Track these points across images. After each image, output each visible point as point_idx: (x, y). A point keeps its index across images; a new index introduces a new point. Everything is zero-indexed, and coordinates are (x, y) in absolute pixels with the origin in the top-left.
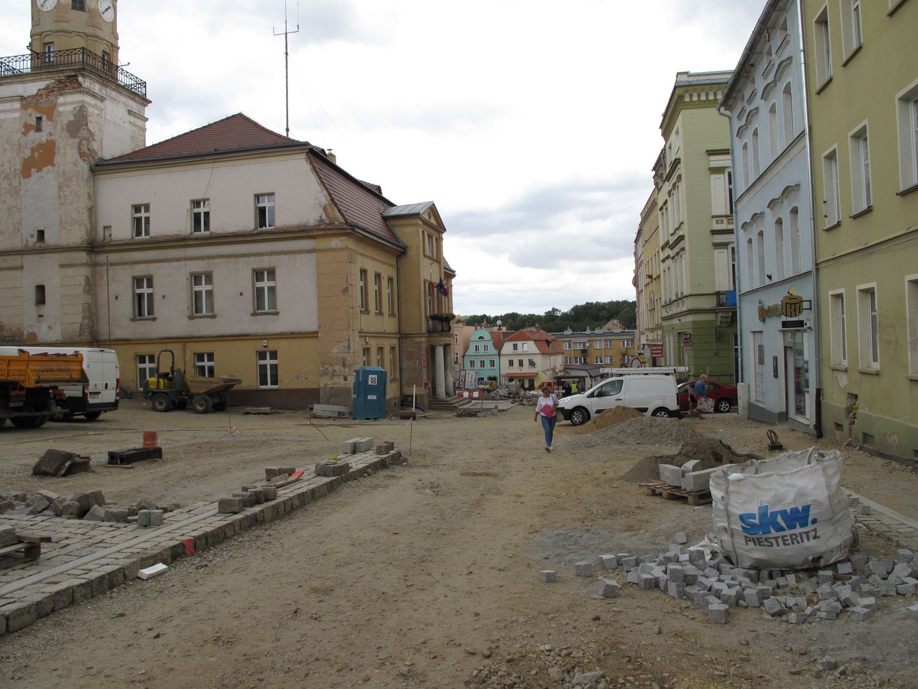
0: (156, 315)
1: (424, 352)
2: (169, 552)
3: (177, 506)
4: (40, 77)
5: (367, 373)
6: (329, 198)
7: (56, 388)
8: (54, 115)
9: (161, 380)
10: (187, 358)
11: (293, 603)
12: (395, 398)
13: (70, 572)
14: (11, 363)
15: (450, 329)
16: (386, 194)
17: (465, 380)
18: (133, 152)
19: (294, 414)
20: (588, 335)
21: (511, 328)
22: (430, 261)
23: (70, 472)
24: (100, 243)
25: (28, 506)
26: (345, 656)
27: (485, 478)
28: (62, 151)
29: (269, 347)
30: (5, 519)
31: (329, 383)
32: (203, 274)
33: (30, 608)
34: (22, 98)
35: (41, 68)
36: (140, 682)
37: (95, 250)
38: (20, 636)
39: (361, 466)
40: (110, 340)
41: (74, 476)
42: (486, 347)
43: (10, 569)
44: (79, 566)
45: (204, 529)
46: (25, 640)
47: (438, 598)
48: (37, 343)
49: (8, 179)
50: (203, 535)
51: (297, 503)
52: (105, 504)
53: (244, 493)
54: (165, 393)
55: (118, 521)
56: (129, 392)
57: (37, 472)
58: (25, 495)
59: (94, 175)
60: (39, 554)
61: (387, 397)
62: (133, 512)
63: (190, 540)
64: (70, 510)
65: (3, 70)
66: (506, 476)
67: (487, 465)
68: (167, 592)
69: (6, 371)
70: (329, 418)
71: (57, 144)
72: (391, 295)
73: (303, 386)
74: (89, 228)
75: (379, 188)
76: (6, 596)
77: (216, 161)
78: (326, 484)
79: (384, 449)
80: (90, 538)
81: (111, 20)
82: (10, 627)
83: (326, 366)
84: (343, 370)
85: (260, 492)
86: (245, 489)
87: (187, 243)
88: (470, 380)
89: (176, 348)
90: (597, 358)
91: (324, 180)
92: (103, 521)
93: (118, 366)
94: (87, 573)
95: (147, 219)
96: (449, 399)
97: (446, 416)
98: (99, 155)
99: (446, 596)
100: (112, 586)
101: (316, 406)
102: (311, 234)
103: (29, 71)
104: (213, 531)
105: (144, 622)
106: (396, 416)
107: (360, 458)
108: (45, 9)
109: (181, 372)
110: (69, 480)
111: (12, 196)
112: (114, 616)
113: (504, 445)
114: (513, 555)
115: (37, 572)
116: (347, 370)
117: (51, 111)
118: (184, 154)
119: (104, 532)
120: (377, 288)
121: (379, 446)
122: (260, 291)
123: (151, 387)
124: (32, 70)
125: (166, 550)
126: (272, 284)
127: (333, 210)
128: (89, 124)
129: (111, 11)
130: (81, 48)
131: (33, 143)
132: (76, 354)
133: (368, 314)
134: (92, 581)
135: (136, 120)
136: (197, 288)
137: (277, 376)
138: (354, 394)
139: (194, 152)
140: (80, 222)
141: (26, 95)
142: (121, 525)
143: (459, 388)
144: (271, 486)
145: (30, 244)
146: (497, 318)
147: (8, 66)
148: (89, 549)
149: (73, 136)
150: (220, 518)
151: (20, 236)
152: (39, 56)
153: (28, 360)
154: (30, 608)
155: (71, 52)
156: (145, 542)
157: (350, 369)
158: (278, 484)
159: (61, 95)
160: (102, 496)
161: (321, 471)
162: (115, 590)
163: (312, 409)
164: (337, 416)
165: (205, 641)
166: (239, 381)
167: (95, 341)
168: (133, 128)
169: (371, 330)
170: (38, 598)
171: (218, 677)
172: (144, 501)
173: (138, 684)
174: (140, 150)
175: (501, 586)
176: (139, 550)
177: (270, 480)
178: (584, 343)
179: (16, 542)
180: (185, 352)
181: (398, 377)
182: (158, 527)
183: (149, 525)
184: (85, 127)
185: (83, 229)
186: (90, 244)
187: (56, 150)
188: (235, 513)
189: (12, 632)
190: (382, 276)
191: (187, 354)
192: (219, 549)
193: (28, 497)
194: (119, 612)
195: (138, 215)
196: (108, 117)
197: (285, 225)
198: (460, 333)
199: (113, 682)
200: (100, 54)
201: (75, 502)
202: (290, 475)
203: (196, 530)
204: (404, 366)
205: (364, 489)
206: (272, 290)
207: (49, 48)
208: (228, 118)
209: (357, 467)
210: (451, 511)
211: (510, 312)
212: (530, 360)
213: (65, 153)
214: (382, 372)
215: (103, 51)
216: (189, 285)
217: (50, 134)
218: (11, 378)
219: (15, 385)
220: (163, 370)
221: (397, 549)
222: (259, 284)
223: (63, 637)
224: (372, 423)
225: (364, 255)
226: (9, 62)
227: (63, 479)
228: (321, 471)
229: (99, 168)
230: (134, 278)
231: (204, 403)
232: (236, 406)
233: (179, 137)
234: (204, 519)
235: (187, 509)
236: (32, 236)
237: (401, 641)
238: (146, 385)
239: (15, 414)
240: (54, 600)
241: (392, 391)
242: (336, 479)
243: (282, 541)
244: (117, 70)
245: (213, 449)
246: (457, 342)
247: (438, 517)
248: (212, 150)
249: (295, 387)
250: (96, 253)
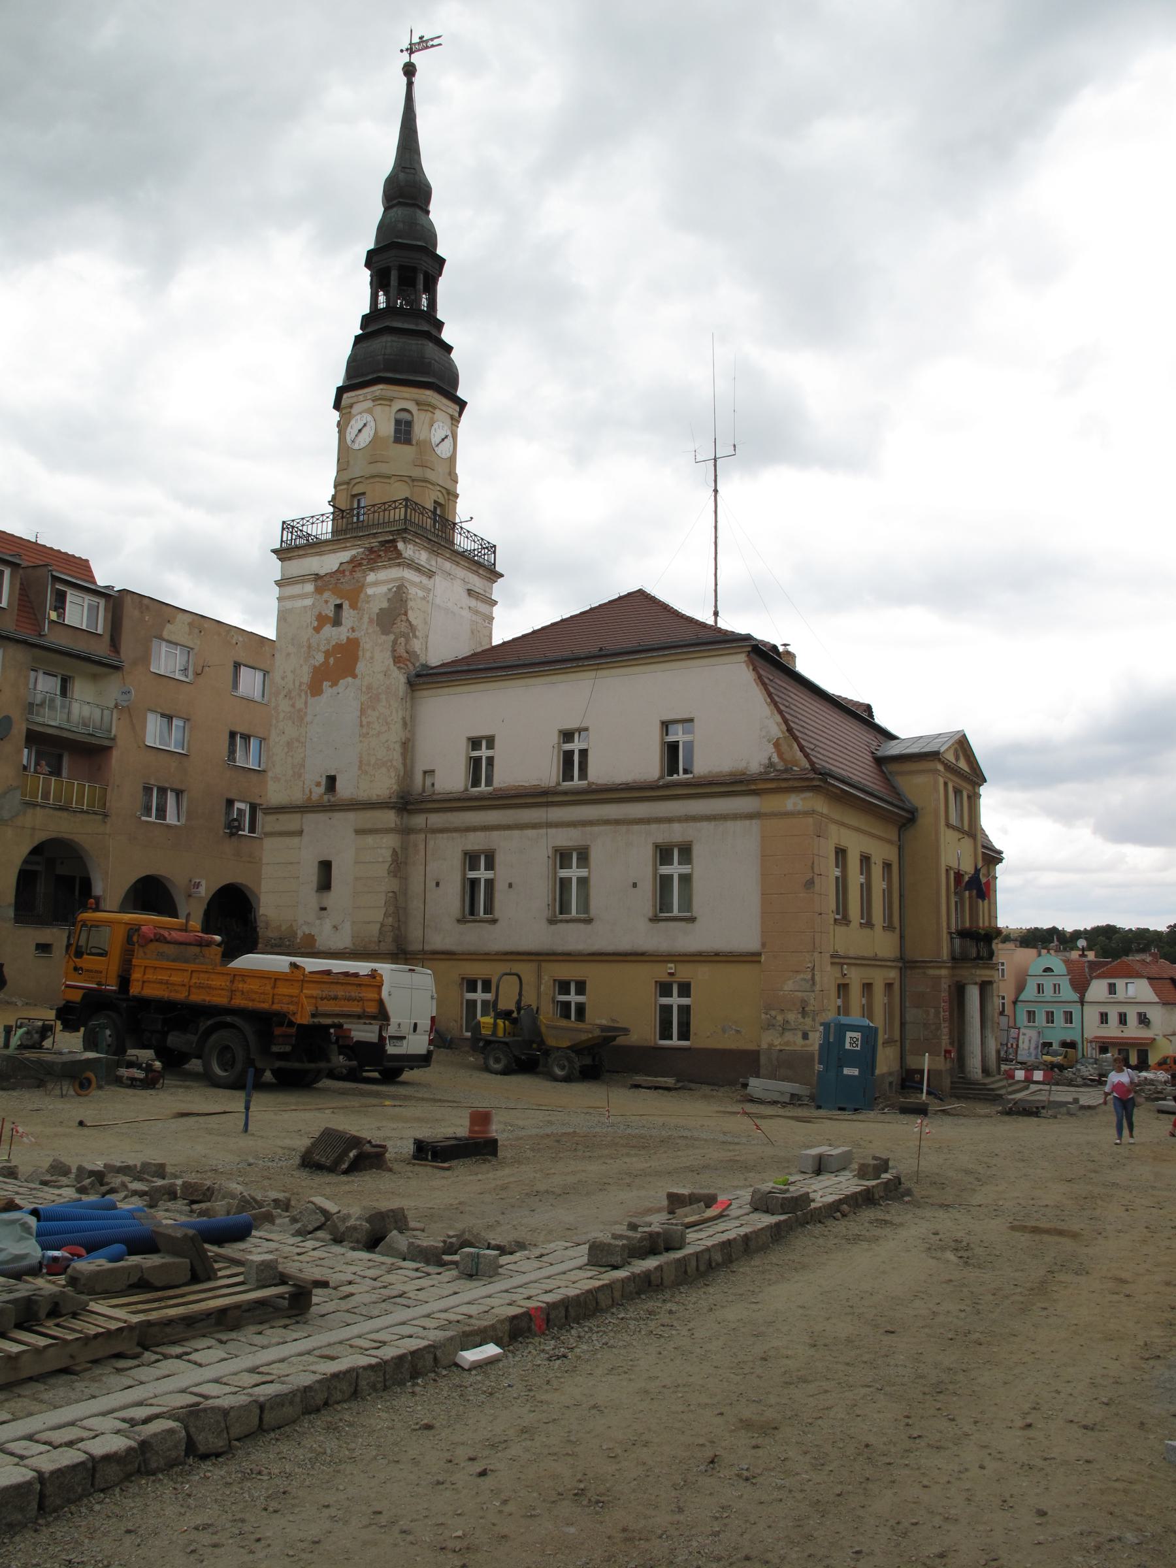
0: (497, 913)
1: (944, 995)
2: (507, 1327)
3: (521, 1246)
4: (343, 545)
5: (842, 1029)
6: (784, 727)
7: (340, 1026)
8: (360, 600)
9: (500, 1022)
10: (543, 987)
11: (707, 1444)
12: (890, 1074)
13: (352, 1342)
14: (279, 983)
15: (991, 954)
16: (880, 719)
17: (1017, 1045)
18: (472, 655)
19: (714, 1093)
21: (1105, 952)
22: (957, 835)
23: (355, 1167)
24: (418, 797)
25: (294, 1220)
26: (798, 1559)
27: (1057, 1238)
28: (368, 654)
29: (677, 976)
30: (260, 1238)
31: (776, 1042)
32: (575, 850)
33: (294, 1395)
34: (317, 577)
35: (345, 531)
36: (455, 1551)
37: (408, 807)
38: (277, 1440)
39: (830, 1199)
40: (423, 952)
41: (361, 1174)
42: (1057, 988)
43: (267, 1326)
44: (368, 1333)
45: (562, 1291)
46: (284, 1447)
47: (967, 1470)
48: (316, 950)
49: (290, 698)
50: (562, 1301)
51: (718, 1257)
52: (408, 1229)
53: (630, 1234)
54: (506, 1043)
55: (428, 1263)
56: (449, 1037)
57: (306, 1163)
58: (289, 1200)
59: (413, 691)
60: (309, 1305)
61: (877, 1072)
62: (451, 1249)
63: (541, 1308)
64: (356, 1235)
65: (294, 537)
66: (1096, 1239)
67: (1059, 1212)
68: (501, 1396)
69: (271, 996)
70: (775, 1103)
71: (361, 645)
72: (888, 893)
73: (733, 1046)
74: (402, 773)
75: (868, 708)
76: (261, 1369)
77: (600, 667)
78: (770, 1227)
79: (870, 1169)
80: (385, 1287)
81: (449, 455)
82: (264, 1423)
83: (773, 1013)
84: (802, 1020)
85: (658, 1234)
86: (633, 1227)
87: (550, 799)
88: (1026, 1046)
89: (526, 970)
91: (776, 698)
92: (404, 1260)
93: (435, 996)
94: (378, 1348)
95: (490, 760)
96: (987, 1081)
97: (982, 1112)
98: (422, 660)
99: (982, 1467)
100: (415, 1374)
101: (753, 1082)
102: (753, 787)
103: (329, 536)
104: (578, 1296)
105: (463, 1444)
106: (892, 1106)
107: (831, 1183)
108: (356, 447)
109: (532, 1009)
110: (353, 1181)
111: (294, 723)
112: (417, 1427)
113: (1093, 1175)
114: (1111, 1399)
115: (306, 1335)
116: (808, 1021)
117: (355, 596)
118: (552, 656)
119: (407, 1279)
120: (863, 881)
121: (863, 1165)
122: (666, 881)
123: (483, 1032)
124: (333, 536)
125: (502, 1322)
126: (685, 869)
127: (791, 747)
128: (410, 613)
129: (449, 441)
130: (404, 499)
131: (329, 643)
132: (374, 974)
133: (847, 925)
134: (386, 1362)
135: (479, 604)
136: (564, 873)
137: (688, 1024)
138: (820, 1063)
139: (566, 654)
140: (389, 764)
141: (322, 572)
142: (431, 1269)
143: (1007, 1060)
144: (676, 1225)
145: (315, 797)
146: (1077, 935)
147: (301, 531)
148: (383, 1305)
149: (385, 631)
150: (590, 1274)
151: (301, 783)
152: (345, 514)
153: (302, 981)
154: (294, 1395)
155: (390, 506)
156: (469, 1303)
157: (814, 1020)
158: (687, 1220)
159: (372, 570)
160: (405, 1217)
161: (762, 1204)
162: (419, 1381)
163: (745, 1085)
164: (787, 1100)
165: (560, 1494)
166: (625, 1031)
167: (402, 954)
168: (474, 618)
169: (852, 953)
170: (307, 1380)
171: (578, 1563)
172: (469, 1231)
173: (450, 1556)
174: (483, 651)
175: (1088, 1462)
176: (460, 1317)
177: (673, 1213)
179: (277, 1281)
180: (539, 977)
181: (897, 1035)
182: (490, 1280)
183: (477, 1275)
184: (404, 617)
185: (393, 774)
186: (402, 798)
187: (360, 653)
188: (615, 1268)
189: (267, 1431)
190: (873, 860)
191: (543, 981)
192: (586, 1329)
193: (293, 1203)
194: (425, 1421)
195: (476, 754)
196: (438, 601)
197: (710, 772)
198: (1010, 958)
199: (412, 1543)
200: (430, 505)
201: (364, 1223)
202: (708, 1206)
203: (550, 1291)
204: (909, 1017)
205: (836, 1241)
206: (686, 879)
207: (359, 500)
208: (620, 598)
209: (824, 1199)
210: (992, 1298)
211: (1102, 922)
212: (1140, 1014)
213: (372, 658)
214: (869, 1027)
215: (435, 502)
216: (550, 867)
217: (353, 630)
218: (276, 1007)
219: (280, 1018)
220: (503, 1005)
221: (893, 1362)
222: (665, 870)
223: (339, 1451)
224: (849, 1117)
225: (843, 824)
226: (303, 525)
227: (344, 1178)
228: (762, 1204)
229: (421, 680)
230: (466, 854)
231: (566, 1064)
232: (618, 1072)
233: (543, 629)
234: (564, 1273)
235: (537, 1252)
236: (318, 784)
237: (898, 1545)
238: (476, 1028)
239: (278, 1064)
240: (329, 1388)
241: (886, 1061)
242: (785, 1221)
243: (691, 1325)
244: (453, 529)
245: (580, 1147)
246: (1003, 976)
247: (968, 1309)
248: (595, 650)
249: (720, 1046)
250: (410, 812)
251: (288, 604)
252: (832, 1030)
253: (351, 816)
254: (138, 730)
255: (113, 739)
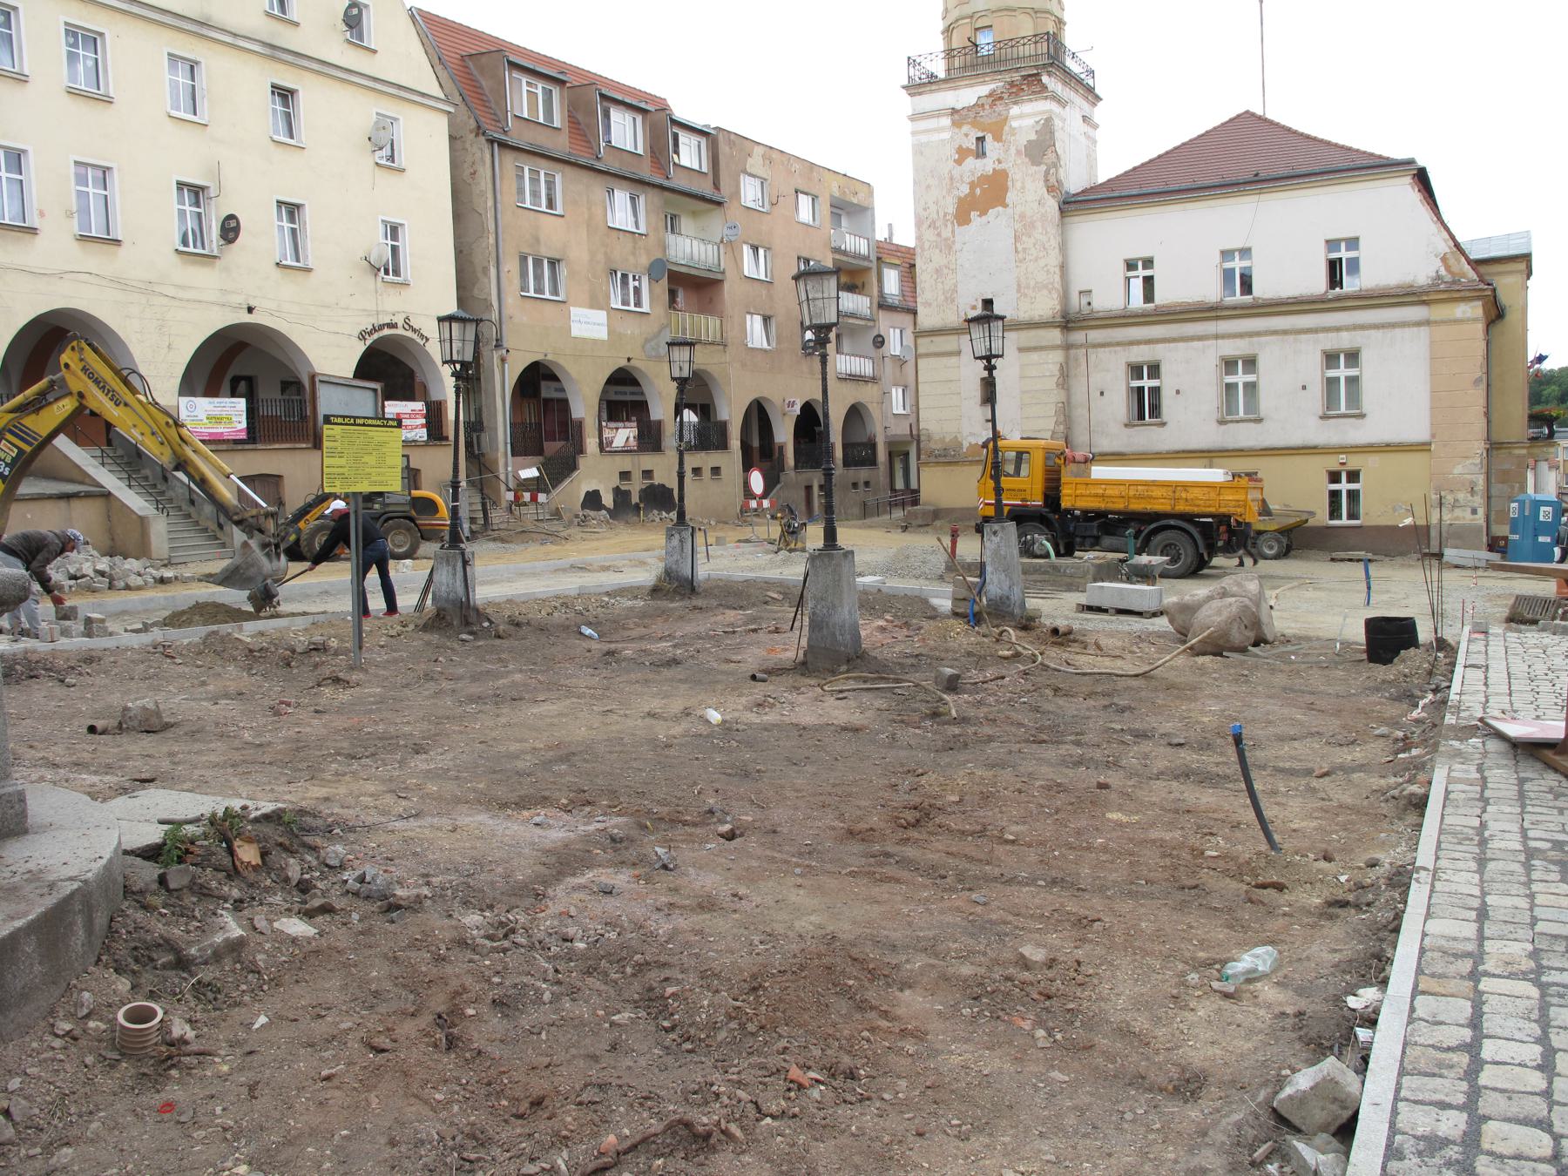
28: (1018, 185)
34: (954, 111)
141: (959, 107)
159: (1015, 103)
187: (1010, 184)
204: (1494, 492)
213: (1023, 188)
251: (923, 138)
252: (1527, 506)
254: (738, 262)
255: (723, 273)
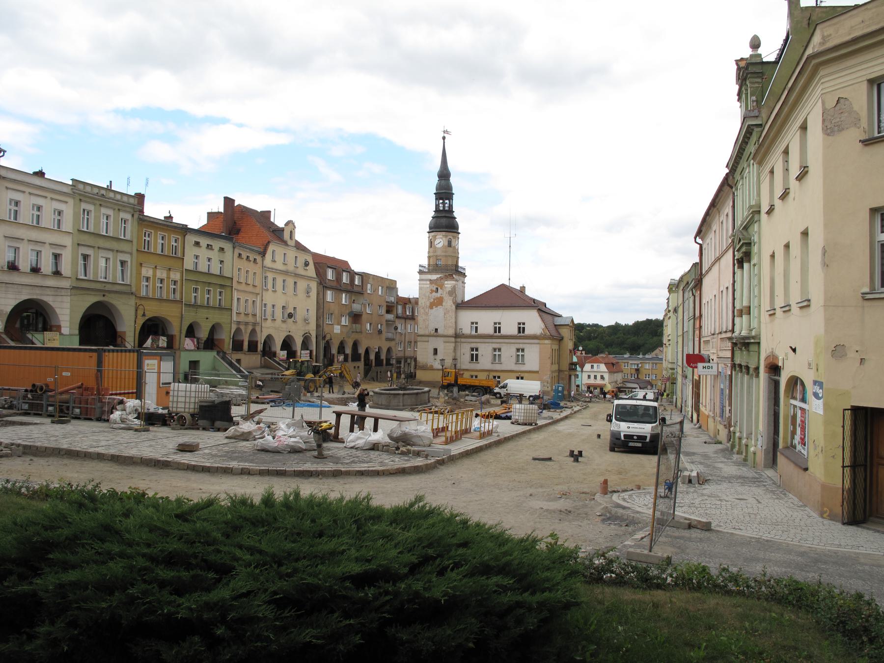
20: (641, 359)
34: (430, 280)
90: (646, 375)
117: (442, 286)
126: (523, 354)
136: (495, 353)
178: (638, 365)
253: (442, 338)
